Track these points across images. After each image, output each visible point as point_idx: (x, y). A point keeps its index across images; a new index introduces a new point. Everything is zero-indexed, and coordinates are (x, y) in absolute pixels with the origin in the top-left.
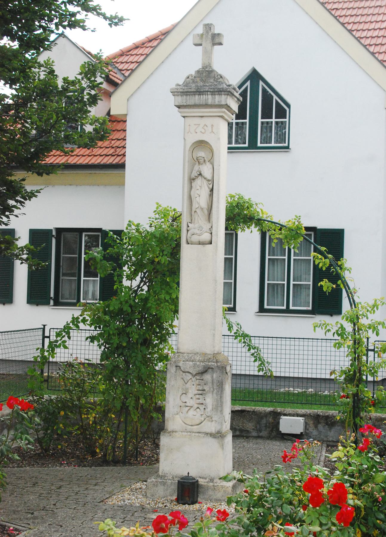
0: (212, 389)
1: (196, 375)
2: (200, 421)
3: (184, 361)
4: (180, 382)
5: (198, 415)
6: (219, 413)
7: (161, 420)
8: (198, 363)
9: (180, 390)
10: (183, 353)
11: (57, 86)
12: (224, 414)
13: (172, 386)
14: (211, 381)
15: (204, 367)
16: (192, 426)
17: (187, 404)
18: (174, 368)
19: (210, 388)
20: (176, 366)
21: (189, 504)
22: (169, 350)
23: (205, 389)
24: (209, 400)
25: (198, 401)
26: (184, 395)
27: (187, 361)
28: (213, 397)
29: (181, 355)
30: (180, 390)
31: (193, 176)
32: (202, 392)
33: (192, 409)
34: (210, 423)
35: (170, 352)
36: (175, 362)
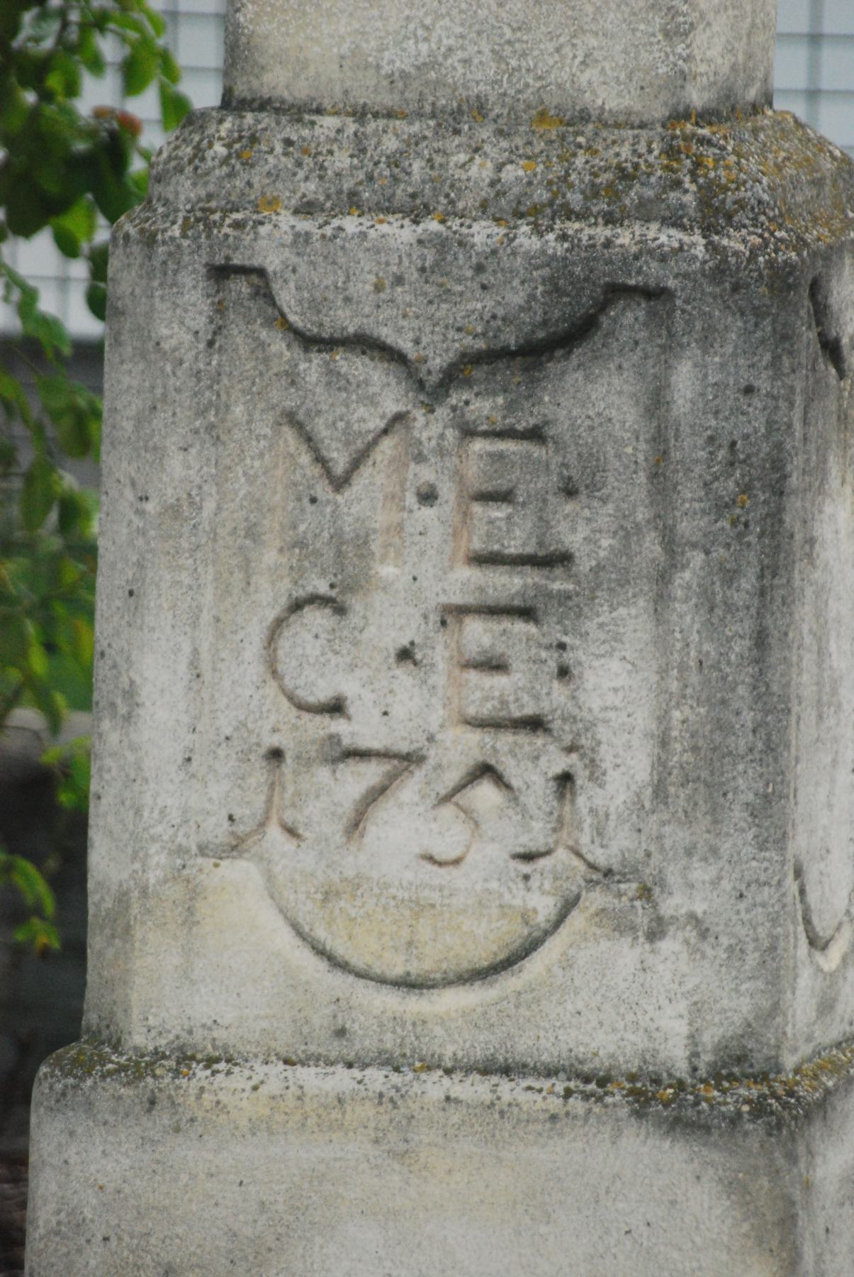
0: (651, 546)
1: (453, 376)
2: (515, 932)
3: (307, 208)
4: (265, 465)
5: (490, 856)
6: (738, 838)
7: (45, 936)
8: (483, 233)
9: (270, 556)
10: (302, 112)
11: (389, 772)
12: (800, 843)
13: (174, 511)
14: (641, 451)
15: (558, 279)
16: (409, 984)
17: (351, 731)
18: (194, 297)
19: (628, 534)
20: (221, 273)
21: (785, 477)
22: (132, 77)
23: (573, 538)
24: (622, 684)
25: (486, 692)
26: (316, 618)
27: (353, 202)
28: (661, 642)
29: (276, 131)
30: (270, 556)
31: (522, 209)
32: (537, 588)
33: (410, 790)
34: (627, 954)
35: (145, 106)
36: (199, 220)
